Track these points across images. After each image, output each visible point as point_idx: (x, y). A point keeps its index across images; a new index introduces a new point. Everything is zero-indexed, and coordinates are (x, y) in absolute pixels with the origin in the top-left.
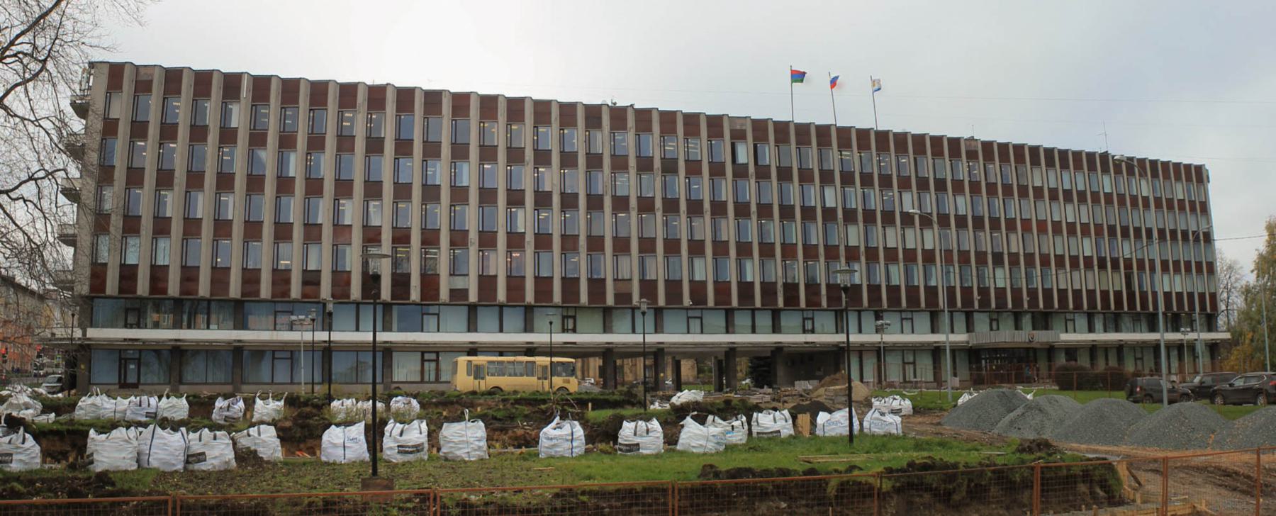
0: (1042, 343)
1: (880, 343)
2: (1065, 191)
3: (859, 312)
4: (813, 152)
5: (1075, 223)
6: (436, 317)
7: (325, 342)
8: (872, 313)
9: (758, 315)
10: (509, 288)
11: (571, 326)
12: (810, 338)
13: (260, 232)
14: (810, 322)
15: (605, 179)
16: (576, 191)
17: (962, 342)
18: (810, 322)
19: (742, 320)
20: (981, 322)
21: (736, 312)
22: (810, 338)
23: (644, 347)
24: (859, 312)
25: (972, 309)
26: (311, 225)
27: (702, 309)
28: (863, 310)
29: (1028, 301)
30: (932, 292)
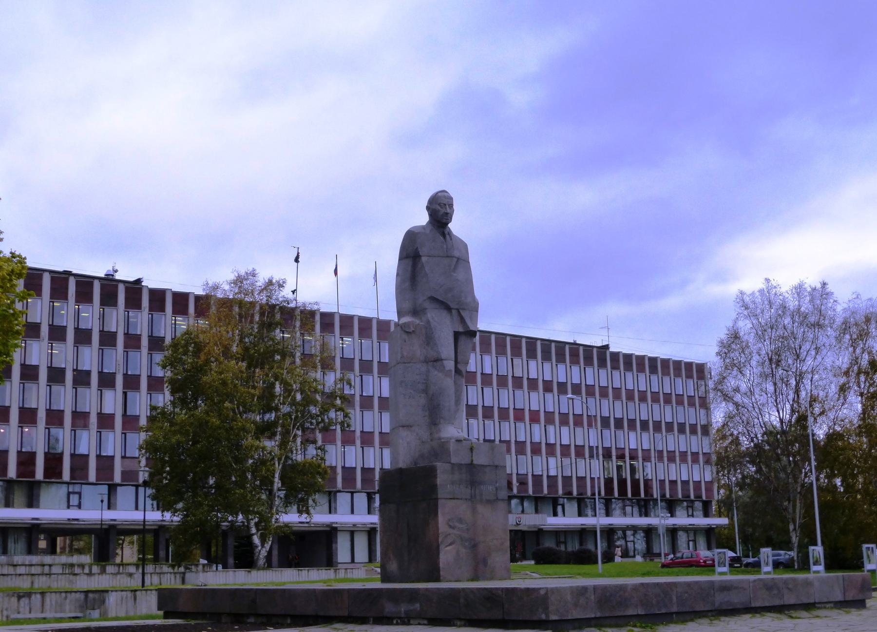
0: (529, 526)
2: (559, 384)
3: (352, 493)
5: (673, 423)
8: (365, 494)
9: (141, 490)
10: (20, 464)
11: (76, 503)
14: (77, 496)
15: (118, 358)
18: (77, 496)
19: (125, 494)
21: (119, 488)
22: (73, 514)
23: (102, 521)
24: (352, 493)
25: (557, 496)
26: (365, 432)
29: (517, 487)
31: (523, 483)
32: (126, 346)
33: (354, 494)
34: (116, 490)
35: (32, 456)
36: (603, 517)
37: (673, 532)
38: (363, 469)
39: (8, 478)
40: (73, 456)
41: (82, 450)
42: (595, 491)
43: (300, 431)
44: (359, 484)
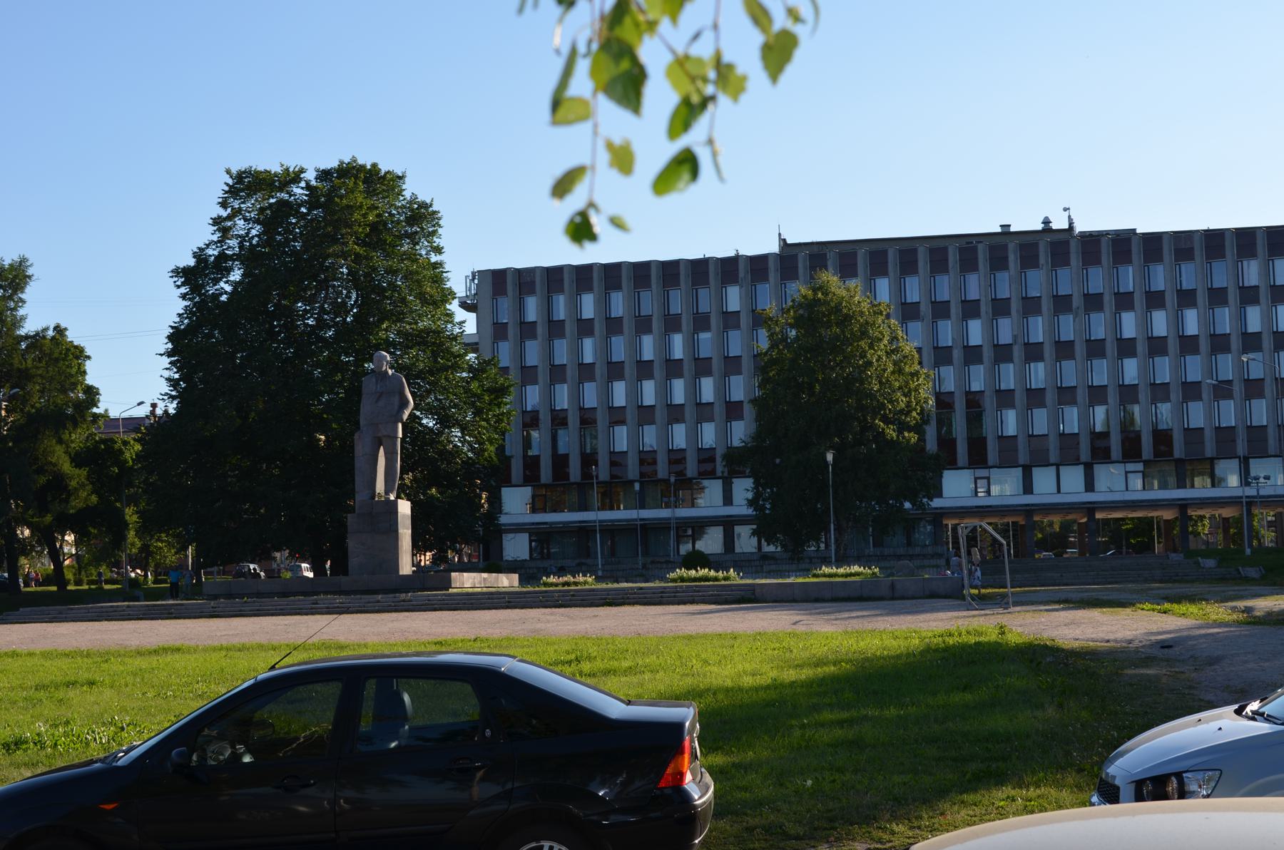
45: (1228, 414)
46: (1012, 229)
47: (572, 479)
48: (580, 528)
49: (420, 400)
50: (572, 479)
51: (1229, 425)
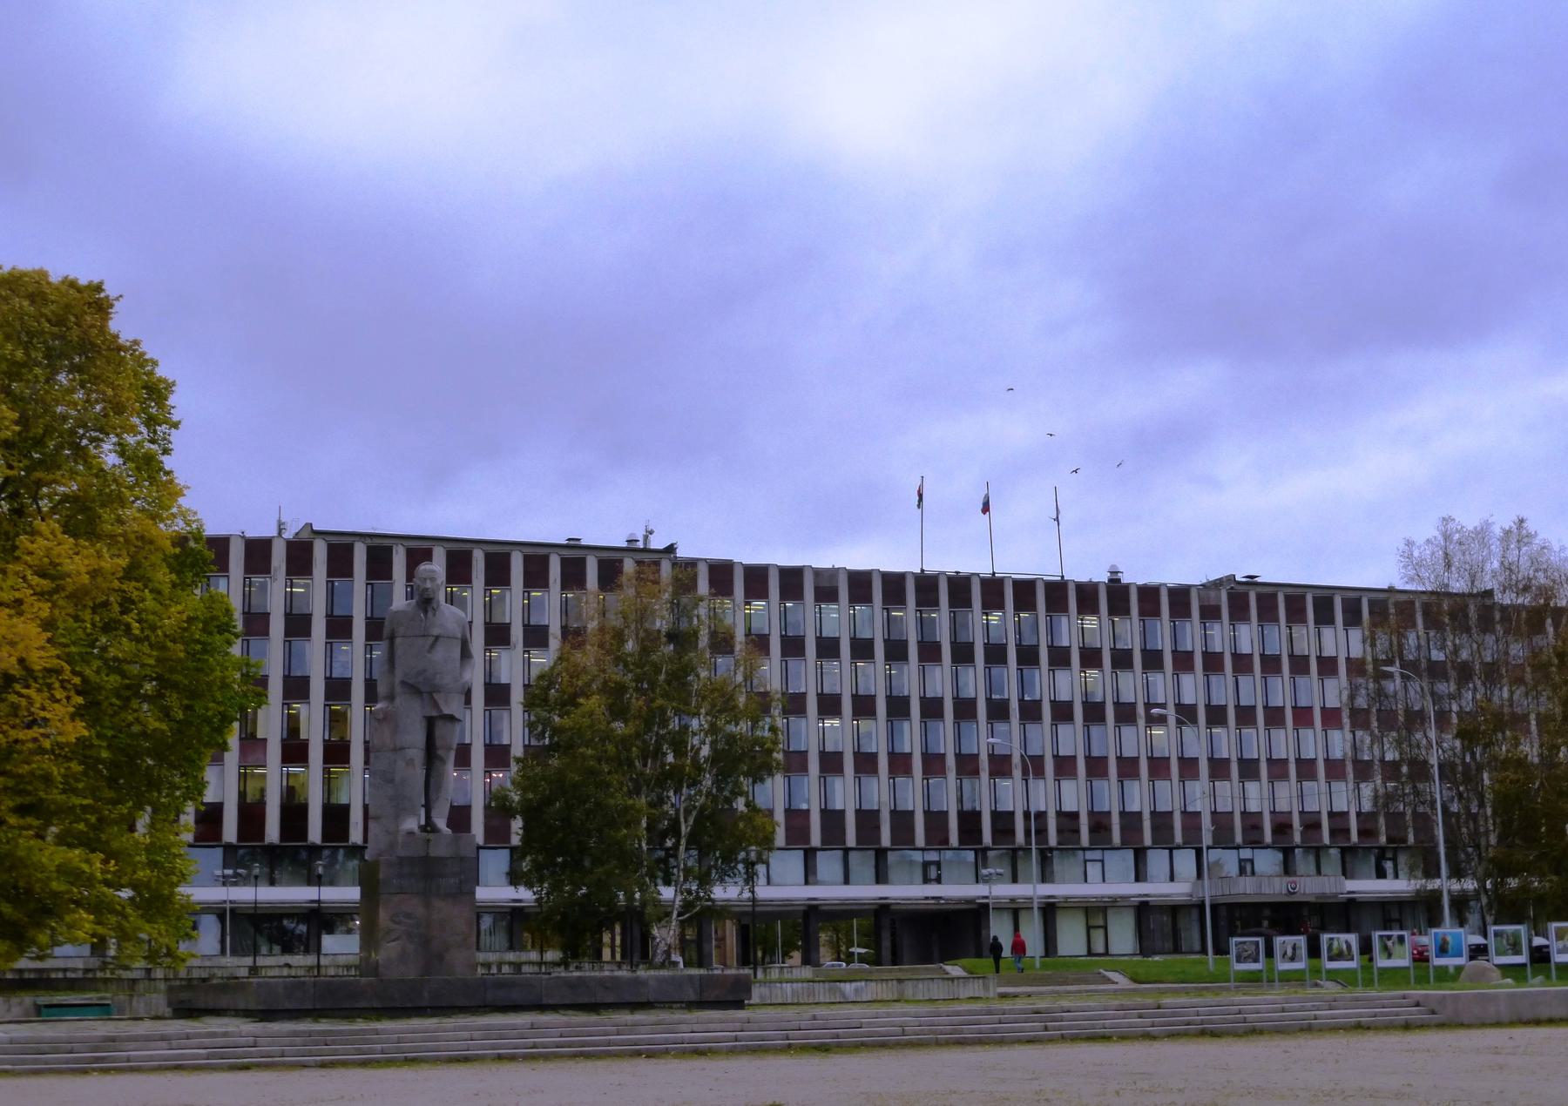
1: (225, 902)
3: (1171, 850)
4: (942, 616)
6: (1100, 864)
7: (312, 902)
12: (933, 890)
13: (1168, 768)
16: (348, 675)
17: (1182, 895)
20: (828, 864)
22: (933, 890)
23: (753, 906)
24: (1171, 850)
27: (1103, 849)
28: (1175, 848)
29: (1302, 833)
30: (1191, 819)
31: (1340, 831)
32: (1020, 661)
33: (1175, 852)
34: (1145, 856)
35: (875, 814)
36: (1008, 883)
37: (1050, 910)
38: (1154, 814)
39: (1016, 846)
40: (1123, 814)
41: (1134, 807)
42: (1433, 838)
43: (512, 755)
44: (1179, 839)
45: (1073, 796)
46: (583, 543)
47: (1409, 843)
48: (514, 909)
49: (675, 715)
50: (1409, 843)
51: (940, 809)
